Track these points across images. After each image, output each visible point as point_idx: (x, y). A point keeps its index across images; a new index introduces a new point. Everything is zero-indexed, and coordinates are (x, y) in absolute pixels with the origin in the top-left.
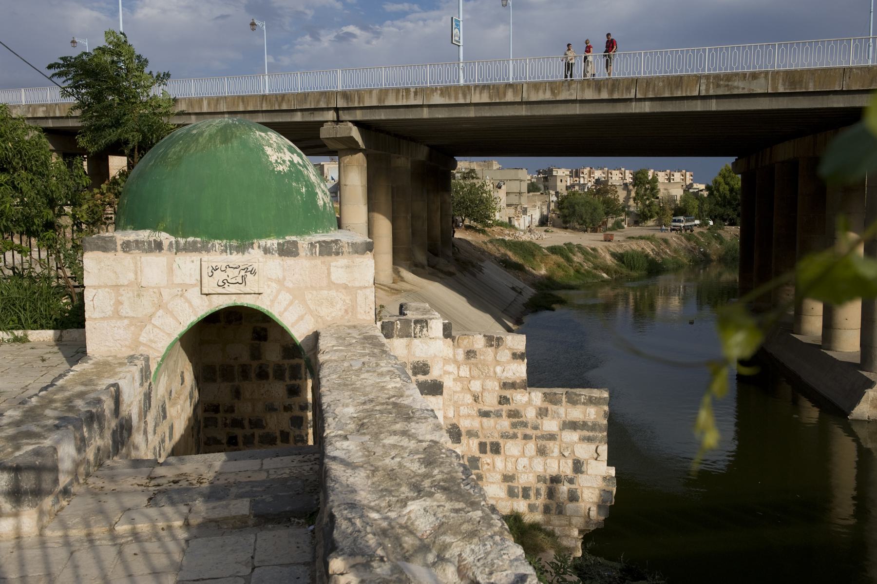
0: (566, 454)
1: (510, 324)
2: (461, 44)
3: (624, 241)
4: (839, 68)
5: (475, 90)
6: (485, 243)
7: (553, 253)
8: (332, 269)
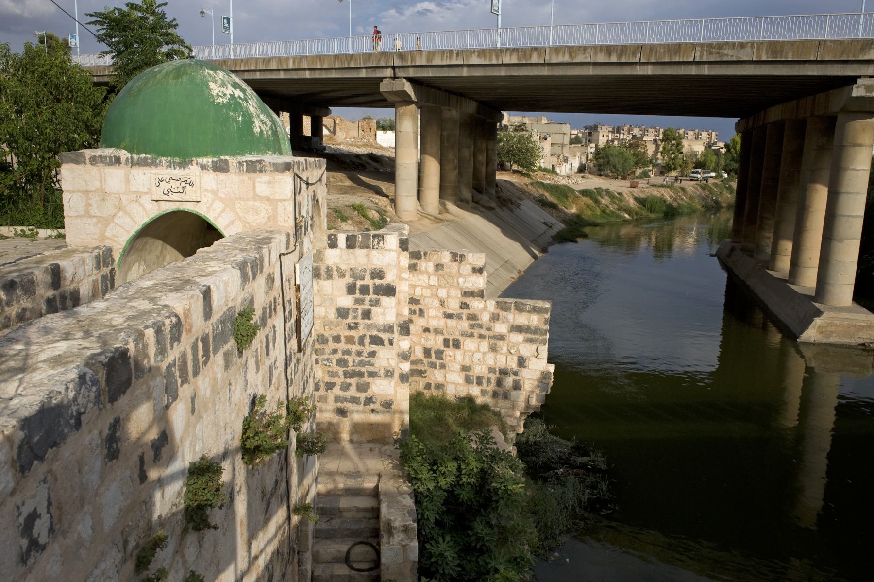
0: (513, 352)
1: (536, 252)
2: (500, 13)
3: (647, 188)
4: (815, 41)
5: (506, 52)
6: (527, 185)
7: (584, 195)
8: (257, 184)
